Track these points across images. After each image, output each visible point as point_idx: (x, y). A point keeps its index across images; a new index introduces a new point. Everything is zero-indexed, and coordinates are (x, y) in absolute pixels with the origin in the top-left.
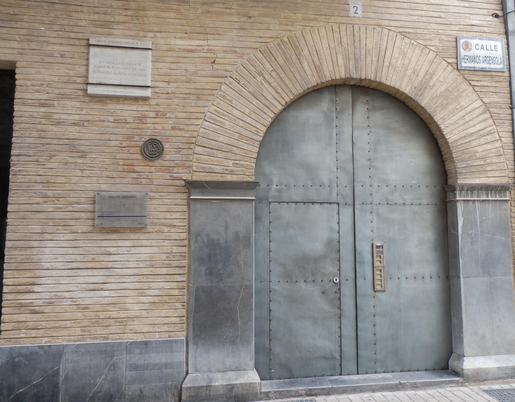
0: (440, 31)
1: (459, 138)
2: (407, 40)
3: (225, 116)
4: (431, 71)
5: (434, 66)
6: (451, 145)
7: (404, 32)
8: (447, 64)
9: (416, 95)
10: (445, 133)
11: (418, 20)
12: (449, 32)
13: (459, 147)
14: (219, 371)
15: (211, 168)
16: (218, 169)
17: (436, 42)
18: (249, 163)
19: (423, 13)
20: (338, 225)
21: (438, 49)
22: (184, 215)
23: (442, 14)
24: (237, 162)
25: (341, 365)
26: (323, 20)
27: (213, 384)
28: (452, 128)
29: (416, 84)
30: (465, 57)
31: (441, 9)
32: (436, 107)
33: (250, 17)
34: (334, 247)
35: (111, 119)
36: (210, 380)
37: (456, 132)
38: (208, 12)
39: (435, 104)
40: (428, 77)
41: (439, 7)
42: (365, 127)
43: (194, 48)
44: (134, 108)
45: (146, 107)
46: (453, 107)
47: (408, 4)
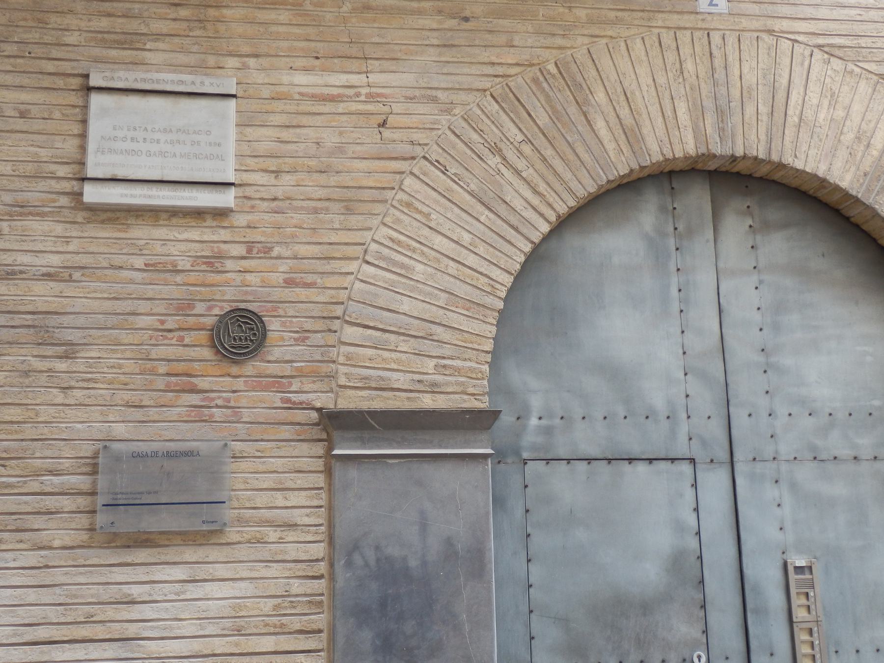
2: (836, 64)
11: (859, 18)
15: (382, 378)
16: (400, 380)
20: (695, 515)
33: (466, 19)
35: (139, 262)
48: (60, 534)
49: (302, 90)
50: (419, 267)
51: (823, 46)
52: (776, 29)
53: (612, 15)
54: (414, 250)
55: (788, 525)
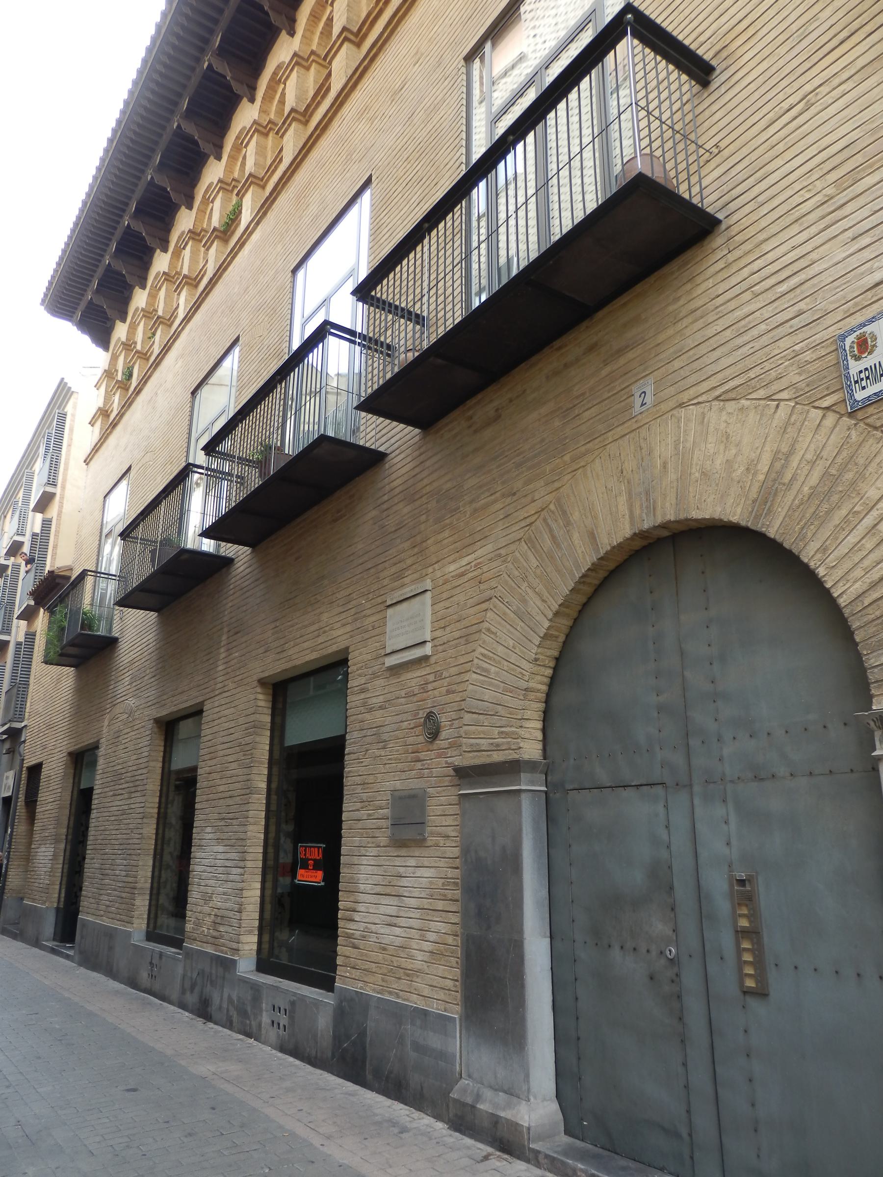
0: (797, 348)
1: (865, 587)
2: (731, 406)
3: (490, 659)
4: (785, 448)
5: (791, 432)
6: (847, 612)
7: (724, 393)
8: (820, 413)
9: (757, 517)
10: (828, 585)
11: (752, 351)
12: (818, 338)
13: (870, 610)
14: (491, 1087)
15: (478, 744)
16: (484, 743)
17: (793, 377)
18: (513, 729)
19: (763, 327)
20: (666, 832)
21: (797, 390)
22: (455, 820)
23: (802, 306)
24: (503, 729)
25: (692, 1158)
26: (597, 447)
27: (478, 1106)
28: (847, 565)
29: (753, 494)
30: (863, 375)
31: (802, 293)
32: (803, 528)
33: (514, 494)
34: (661, 880)
35: (403, 693)
36: (478, 1097)
37: (858, 572)
38: (476, 510)
39: (801, 520)
40: (778, 465)
41: (798, 291)
42: (698, 613)
43: (463, 569)
44: (418, 673)
45: (428, 668)
46: (844, 512)
47: (733, 327)
48: (384, 841)
49: (452, 574)
50: (493, 669)
51: (720, 396)
52: (685, 401)
53: (583, 449)
54: (490, 659)
55: (734, 842)
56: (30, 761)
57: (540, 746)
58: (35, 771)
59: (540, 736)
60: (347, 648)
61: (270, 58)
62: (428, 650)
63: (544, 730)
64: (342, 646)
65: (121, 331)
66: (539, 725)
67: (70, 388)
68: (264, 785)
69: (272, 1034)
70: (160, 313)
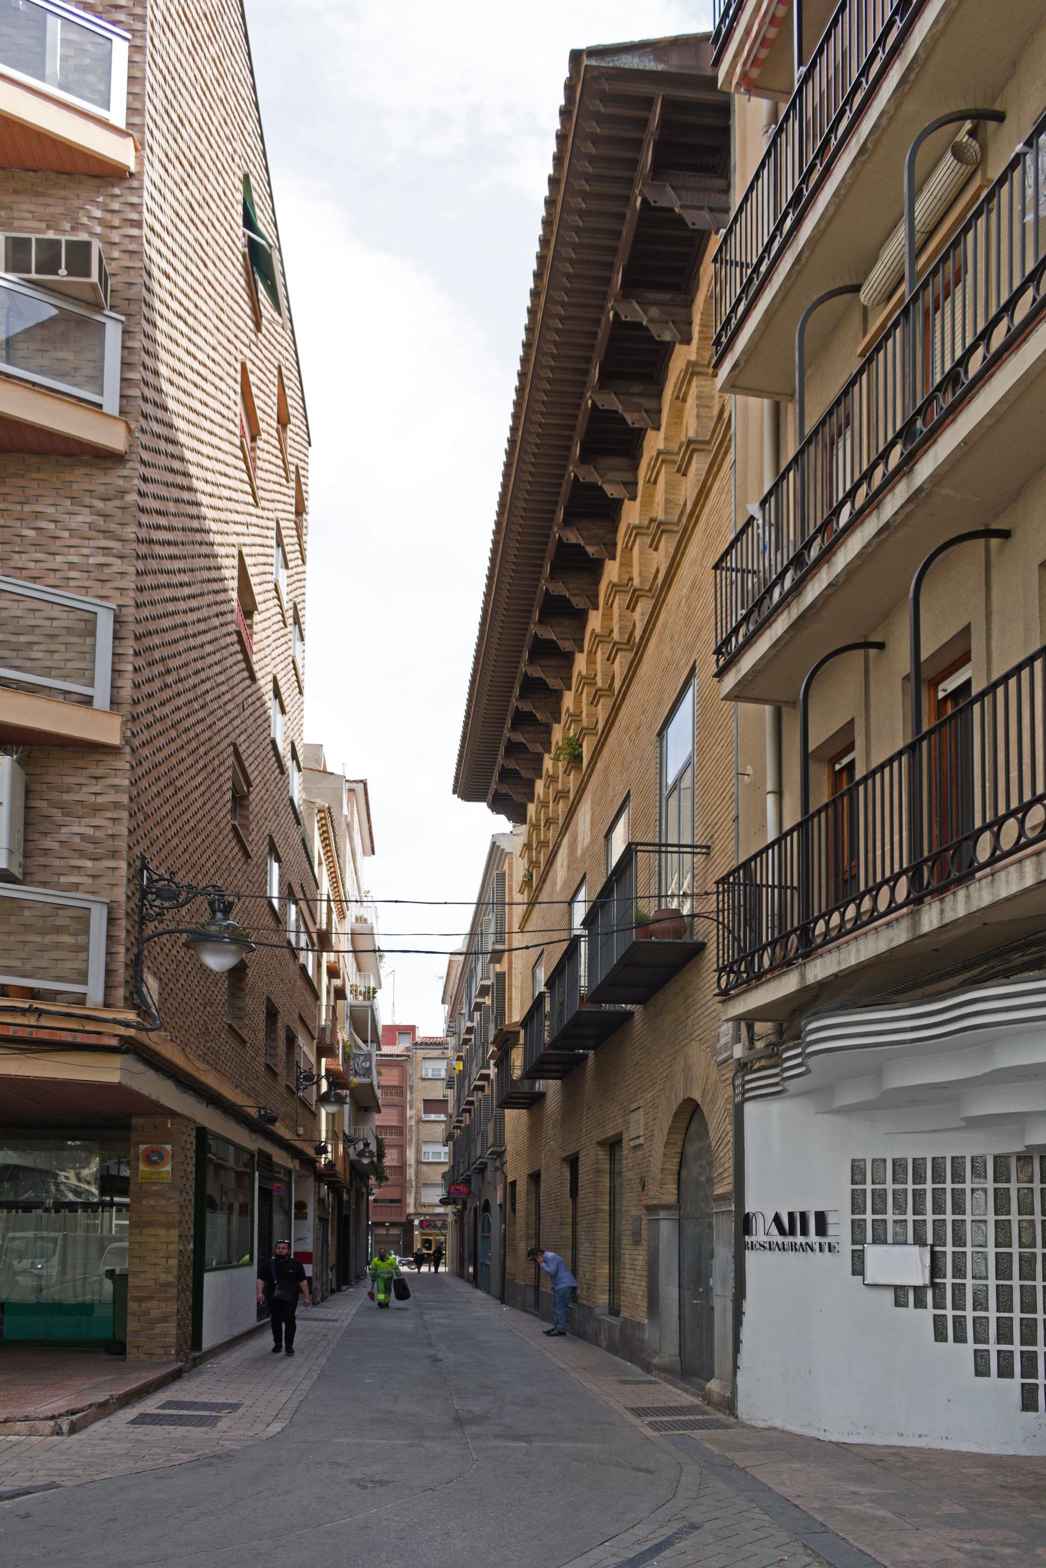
56: (510, 1179)
57: (676, 1197)
58: (513, 1184)
59: (675, 1192)
60: (577, 1153)
61: (671, 365)
62: (641, 1141)
63: (678, 1189)
64: (618, 1131)
65: (531, 809)
66: (675, 1186)
67: (503, 850)
68: (607, 1208)
69: (604, 1344)
70: (636, 582)
